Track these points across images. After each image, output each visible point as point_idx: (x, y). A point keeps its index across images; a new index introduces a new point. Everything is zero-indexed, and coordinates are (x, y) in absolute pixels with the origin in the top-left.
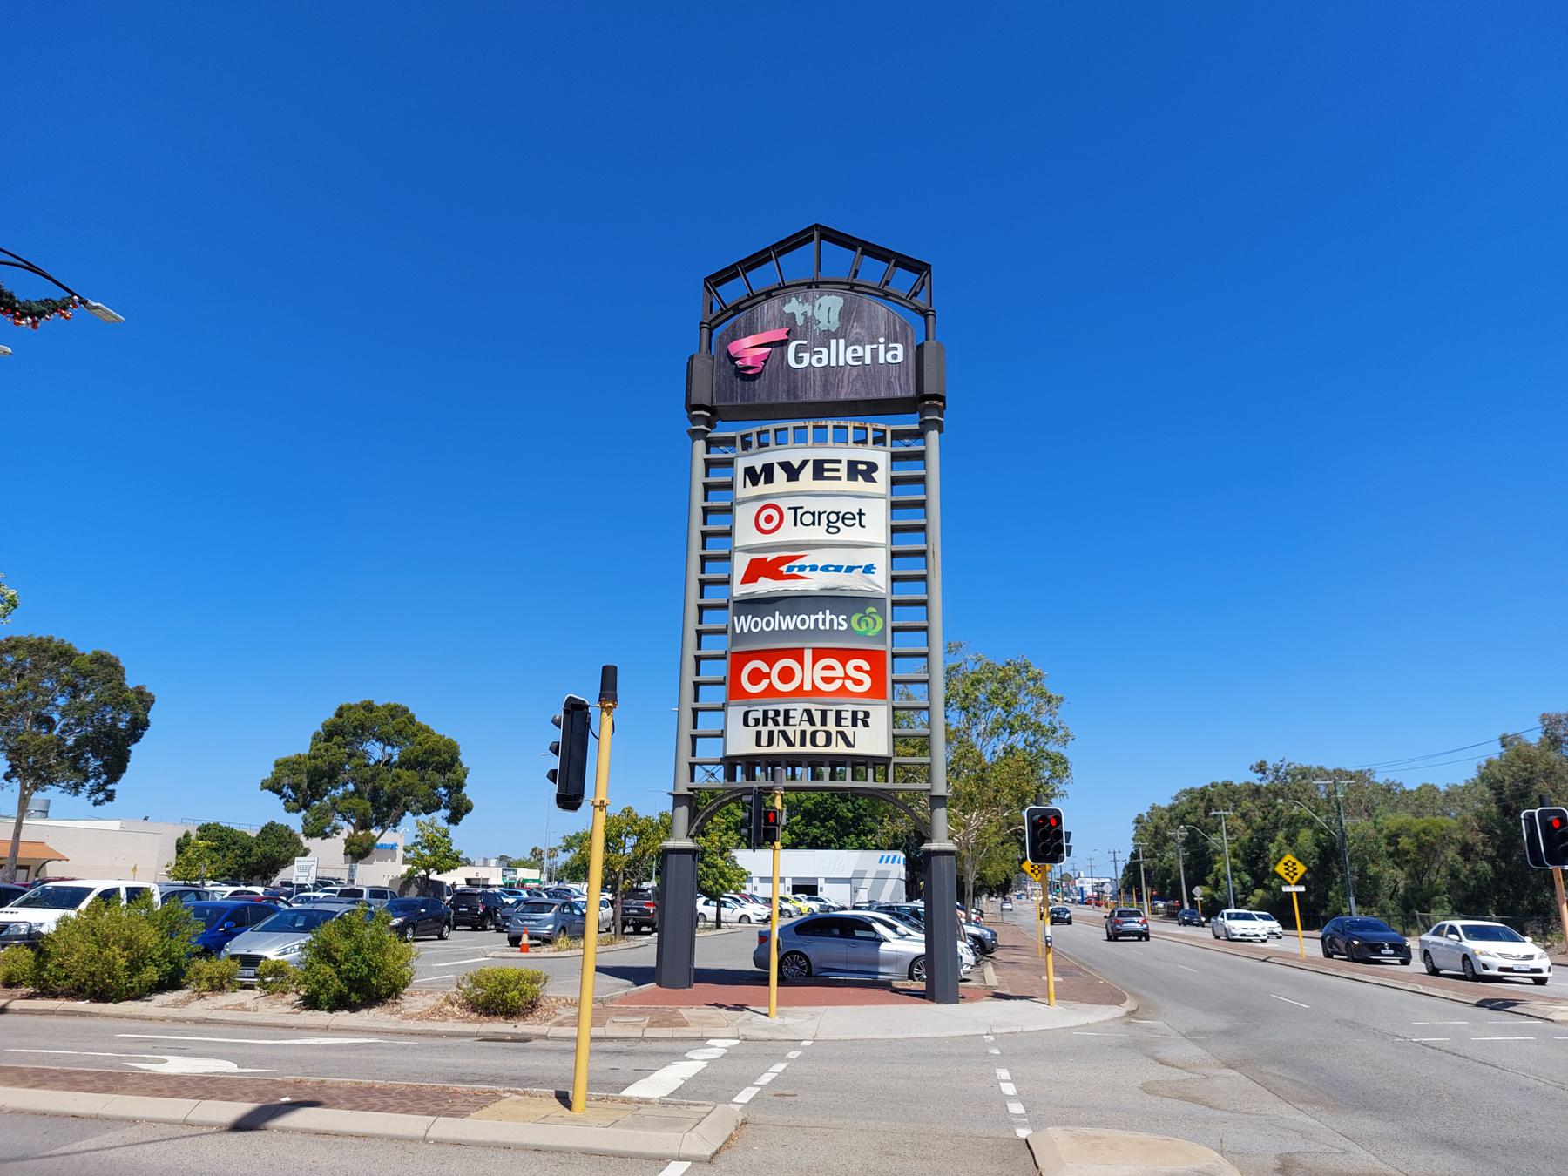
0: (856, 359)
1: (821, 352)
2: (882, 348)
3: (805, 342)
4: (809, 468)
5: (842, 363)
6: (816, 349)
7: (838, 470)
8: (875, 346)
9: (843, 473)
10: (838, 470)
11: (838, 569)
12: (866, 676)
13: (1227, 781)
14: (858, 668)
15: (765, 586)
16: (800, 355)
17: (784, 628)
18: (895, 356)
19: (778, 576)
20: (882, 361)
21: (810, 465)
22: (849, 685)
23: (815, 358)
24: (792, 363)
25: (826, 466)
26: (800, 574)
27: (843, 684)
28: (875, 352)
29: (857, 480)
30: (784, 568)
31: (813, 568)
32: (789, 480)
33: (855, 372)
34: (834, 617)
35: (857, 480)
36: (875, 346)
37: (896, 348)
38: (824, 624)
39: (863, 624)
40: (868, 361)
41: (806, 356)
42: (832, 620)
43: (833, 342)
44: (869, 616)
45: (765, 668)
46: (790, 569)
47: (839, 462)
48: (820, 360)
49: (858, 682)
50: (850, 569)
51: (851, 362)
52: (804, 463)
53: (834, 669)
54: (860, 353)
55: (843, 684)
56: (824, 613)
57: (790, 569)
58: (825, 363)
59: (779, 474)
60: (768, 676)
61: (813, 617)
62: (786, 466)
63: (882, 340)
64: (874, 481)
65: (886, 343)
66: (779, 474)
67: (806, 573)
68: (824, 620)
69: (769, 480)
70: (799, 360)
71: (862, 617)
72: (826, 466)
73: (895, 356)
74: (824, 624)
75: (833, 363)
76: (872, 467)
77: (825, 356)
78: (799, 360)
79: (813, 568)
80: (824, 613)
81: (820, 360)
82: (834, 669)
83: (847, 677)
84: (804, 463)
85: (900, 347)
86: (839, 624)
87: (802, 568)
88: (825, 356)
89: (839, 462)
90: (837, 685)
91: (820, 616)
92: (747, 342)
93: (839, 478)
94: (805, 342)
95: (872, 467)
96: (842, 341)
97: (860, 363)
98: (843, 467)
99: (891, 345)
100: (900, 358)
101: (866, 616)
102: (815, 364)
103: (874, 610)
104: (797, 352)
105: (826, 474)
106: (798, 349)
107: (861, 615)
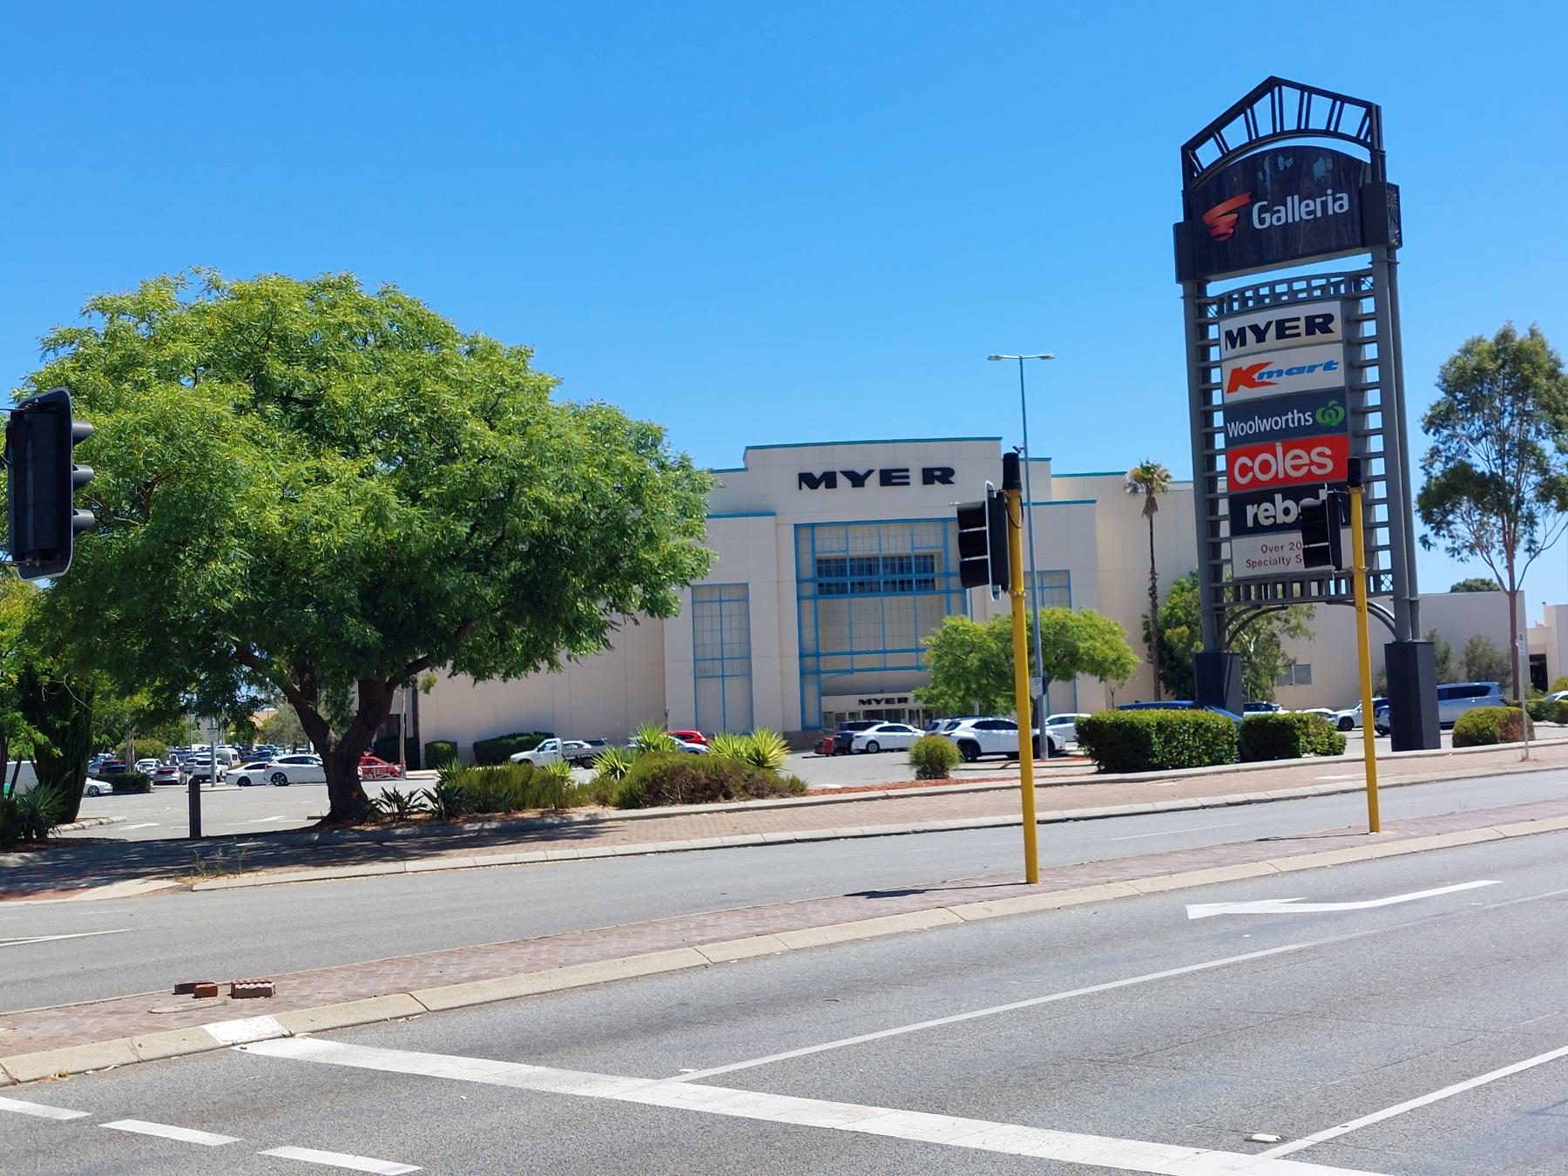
0: (1309, 213)
1: (1279, 211)
2: (1330, 199)
3: (1265, 203)
4: (1273, 330)
5: (1297, 219)
6: (1275, 208)
7: (1297, 327)
8: (1324, 198)
9: (1302, 329)
10: (1297, 327)
11: (1301, 370)
12: (1329, 460)
13: (1480, 638)
14: (1321, 454)
15: (1244, 393)
16: (1263, 216)
17: (1262, 430)
18: (1341, 206)
19: (1252, 384)
20: (1330, 212)
21: (1273, 327)
22: (1315, 469)
23: (1275, 216)
24: (1257, 226)
25: (1287, 325)
26: (1269, 380)
27: (1310, 470)
28: (1324, 205)
29: (1314, 333)
30: (1256, 376)
31: (1280, 373)
32: (1258, 341)
33: (1309, 227)
34: (1301, 415)
35: (1314, 333)
36: (1324, 198)
37: (1341, 198)
38: (1293, 422)
39: (1327, 417)
40: (1319, 214)
41: (1267, 216)
42: (1299, 418)
43: (1289, 199)
44: (1332, 408)
45: (1250, 463)
46: (1261, 376)
47: (1298, 319)
48: (1279, 219)
49: (1322, 466)
50: (1312, 369)
51: (1305, 217)
52: (1269, 324)
53: (1301, 458)
54: (1312, 208)
55: (1310, 470)
56: (1293, 413)
57: (1261, 376)
58: (1283, 221)
59: (1250, 336)
60: (1251, 469)
61: (1284, 418)
62: (1255, 328)
63: (1329, 192)
64: (1331, 331)
65: (1333, 195)
66: (1250, 336)
67: (1274, 379)
68: (1293, 419)
69: (1243, 343)
70: (1262, 221)
71: (1324, 411)
72: (1287, 325)
73: (1341, 206)
74: (1293, 422)
75: (1290, 221)
76: (1329, 318)
77: (1282, 214)
78: (1262, 221)
79: (1280, 373)
80: (1293, 413)
81: (1279, 219)
82: (1301, 458)
83: (1312, 463)
84: (1269, 324)
85: (1345, 196)
86: (1306, 421)
87: (1270, 374)
88: (1282, 214)
89: (1298, 319)
90: (1304, 470)
91: (1290, 416)
92: (1220, 209)
93: (1298, 335)
94: (1265, 203)
95: (1329, 318)
96: (1296, 197)
97: (1312, 216)
98: (1302, 324)
99: (1338, 196)
100: (1346, 208)
101: (1328, 409)
102: (1275, 223)
103: (1336, 402)
104: (1259, 215)
105: (1287, 332)
106: (1262, 210)
107: (1324, 409)
